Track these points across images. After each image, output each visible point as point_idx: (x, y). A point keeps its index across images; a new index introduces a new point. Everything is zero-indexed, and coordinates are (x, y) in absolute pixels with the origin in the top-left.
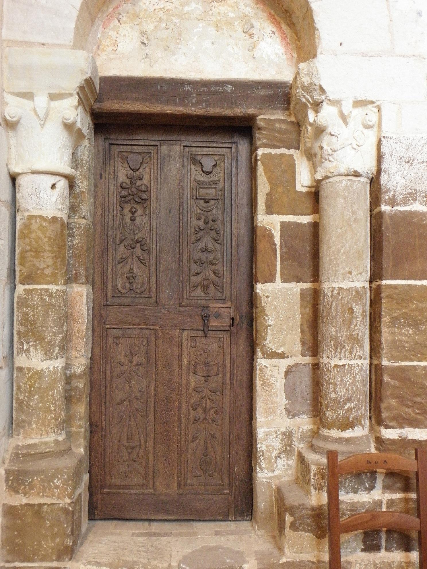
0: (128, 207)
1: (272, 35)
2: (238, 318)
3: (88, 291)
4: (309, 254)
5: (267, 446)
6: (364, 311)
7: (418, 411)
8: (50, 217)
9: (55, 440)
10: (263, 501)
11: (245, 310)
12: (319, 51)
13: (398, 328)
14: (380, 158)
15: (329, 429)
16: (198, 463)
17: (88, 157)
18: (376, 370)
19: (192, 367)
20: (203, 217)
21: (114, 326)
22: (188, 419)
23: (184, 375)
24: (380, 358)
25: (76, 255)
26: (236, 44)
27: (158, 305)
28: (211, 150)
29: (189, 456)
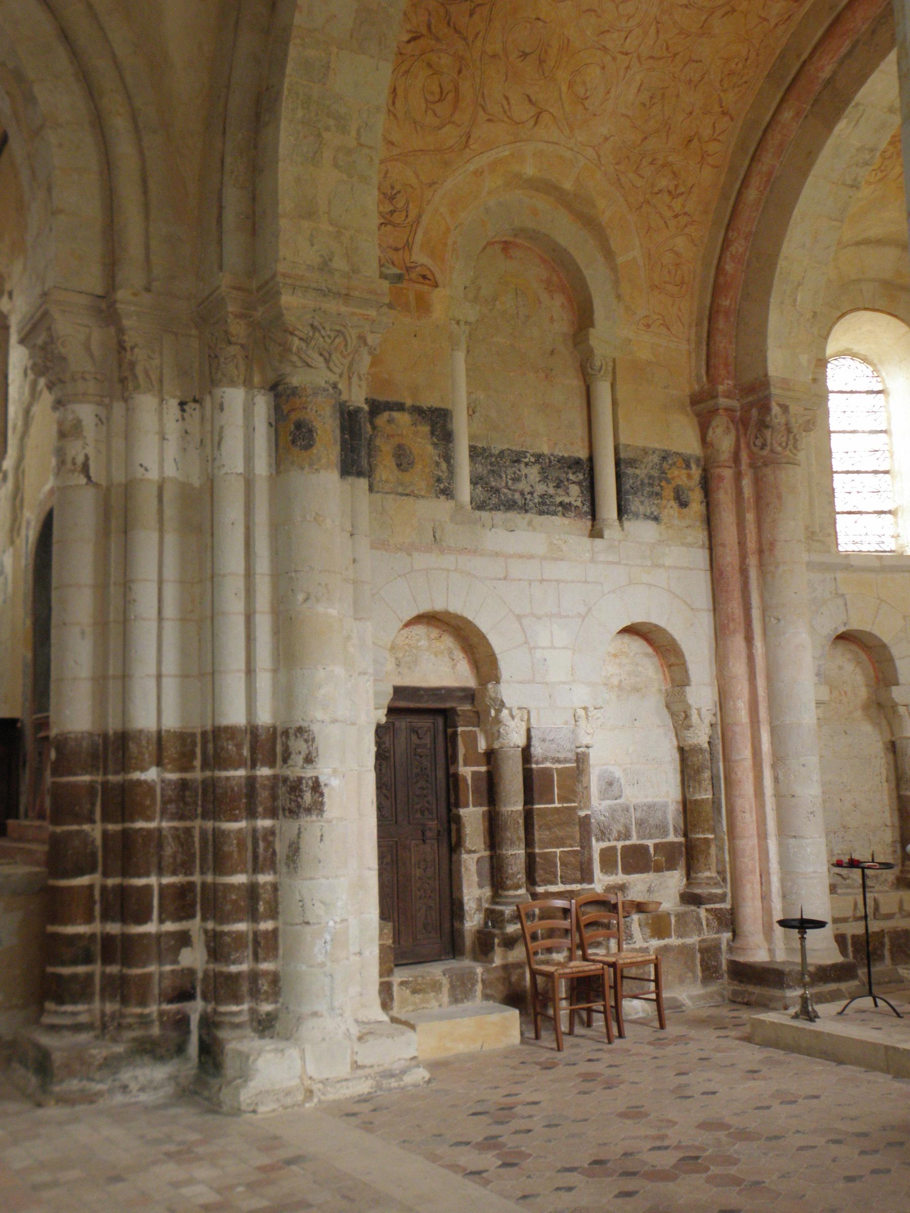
11: (445, 826)
14: (529, 738)
24: (534, 848)
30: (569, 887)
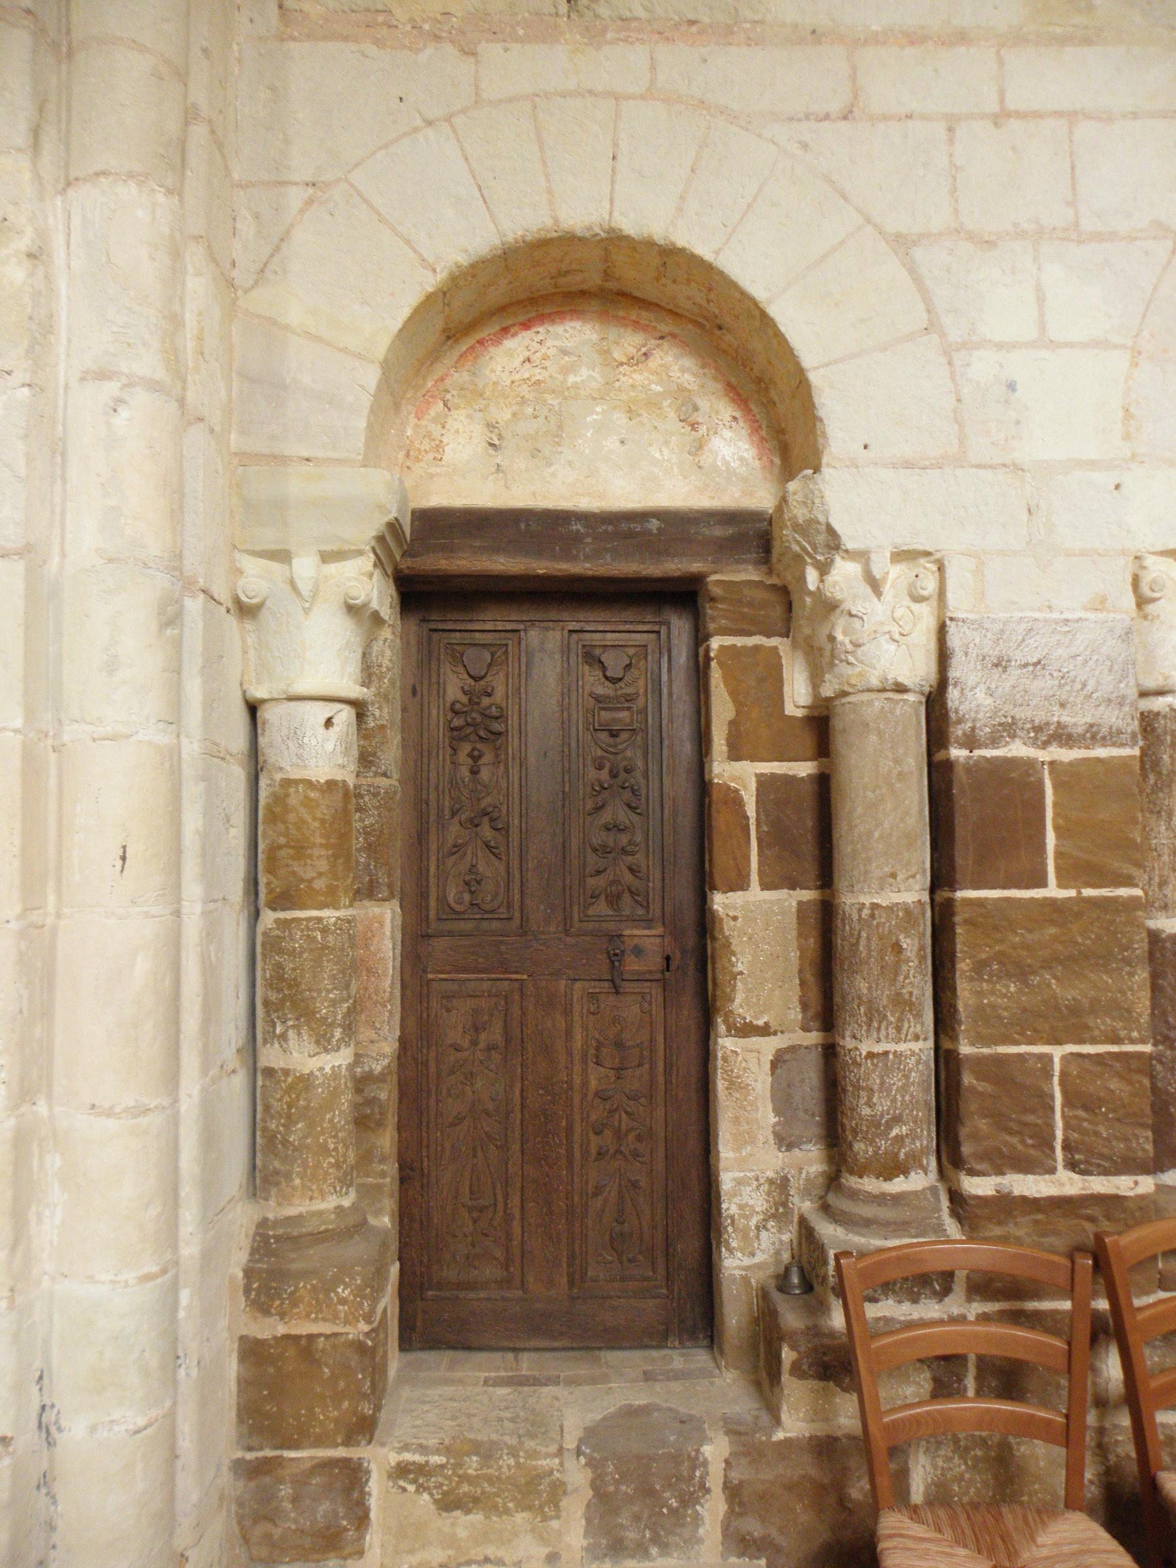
0: (466, 748)
1: (734, 424)
2: (678, 954)
3: (393, 912)
4: (813, 835)
5: (741, 1207)
6: (922, 948)
7: (1030, 1142)
8: (322, 781)
9: (336, 1208)
10: (735, 1315)
11: (691, 941)
12: (825, 460)
13: (986, 981)
14: (943, 657)
15: (861, 1177)
16: (607, 1238)
17: (390, 661)
18: (946, 1063)
19: (592, 1051)
20: (608, 765)
21: (442, 976)
22: (585, 1153)
23: (577, 1068)
24: (954, 1038)
25: (370, 845)
26: (667, 443)
27: (525, 934)
28: (616, 633)
29: (590, 1223)
30: (1099, 1185)
